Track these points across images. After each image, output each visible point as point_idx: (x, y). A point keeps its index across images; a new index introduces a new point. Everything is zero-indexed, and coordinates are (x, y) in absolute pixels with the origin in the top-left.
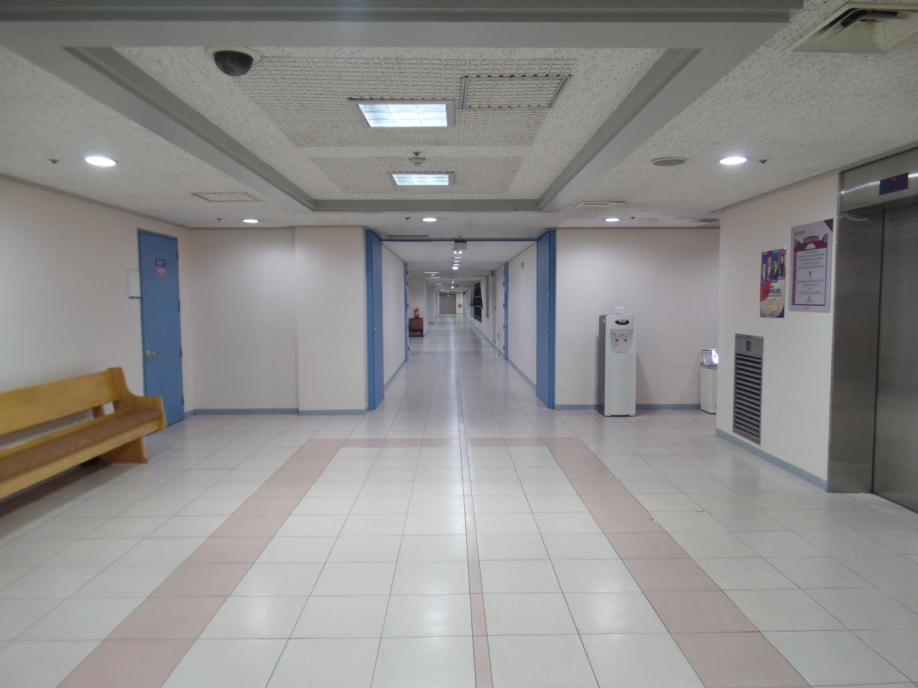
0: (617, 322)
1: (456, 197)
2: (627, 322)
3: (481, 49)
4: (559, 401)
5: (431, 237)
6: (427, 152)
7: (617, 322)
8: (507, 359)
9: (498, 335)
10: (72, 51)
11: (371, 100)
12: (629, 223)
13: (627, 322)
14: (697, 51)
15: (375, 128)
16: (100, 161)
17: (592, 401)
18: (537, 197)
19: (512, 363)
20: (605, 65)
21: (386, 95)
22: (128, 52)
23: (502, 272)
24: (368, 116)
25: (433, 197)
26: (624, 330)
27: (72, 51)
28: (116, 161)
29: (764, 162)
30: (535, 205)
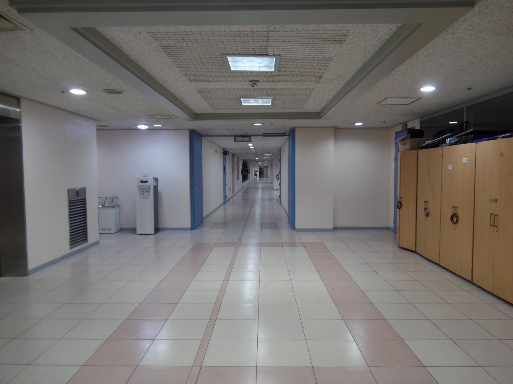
0: (141, 182)
1: (273, 111)
2: (147, 182)
3: (297, 25)
4: (298, 226)
5: (210, 133)
6: (247, 85)
7: (141, 182)
8: (281, 203)
9: (230, 189)
10: (74, 29)
11: (233, 55)
12: (250, 121)
13: (147, 182)
14: (420, 25)
15: (233, 71)
16: (78, 92)
17: (339, 225)
18: (319, 110)
19: (282, 206)
20: (366, 34)
21: (235, 52)
22: (104, 30)
23: (277, 154)
24: (231, 64)
25: (263, 111)
26: (144, 186)
27: (74, 29)
28: (86, 92)
29: (469, 89)
30: (318, 115)
